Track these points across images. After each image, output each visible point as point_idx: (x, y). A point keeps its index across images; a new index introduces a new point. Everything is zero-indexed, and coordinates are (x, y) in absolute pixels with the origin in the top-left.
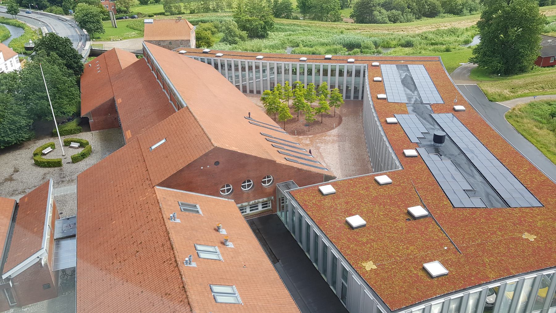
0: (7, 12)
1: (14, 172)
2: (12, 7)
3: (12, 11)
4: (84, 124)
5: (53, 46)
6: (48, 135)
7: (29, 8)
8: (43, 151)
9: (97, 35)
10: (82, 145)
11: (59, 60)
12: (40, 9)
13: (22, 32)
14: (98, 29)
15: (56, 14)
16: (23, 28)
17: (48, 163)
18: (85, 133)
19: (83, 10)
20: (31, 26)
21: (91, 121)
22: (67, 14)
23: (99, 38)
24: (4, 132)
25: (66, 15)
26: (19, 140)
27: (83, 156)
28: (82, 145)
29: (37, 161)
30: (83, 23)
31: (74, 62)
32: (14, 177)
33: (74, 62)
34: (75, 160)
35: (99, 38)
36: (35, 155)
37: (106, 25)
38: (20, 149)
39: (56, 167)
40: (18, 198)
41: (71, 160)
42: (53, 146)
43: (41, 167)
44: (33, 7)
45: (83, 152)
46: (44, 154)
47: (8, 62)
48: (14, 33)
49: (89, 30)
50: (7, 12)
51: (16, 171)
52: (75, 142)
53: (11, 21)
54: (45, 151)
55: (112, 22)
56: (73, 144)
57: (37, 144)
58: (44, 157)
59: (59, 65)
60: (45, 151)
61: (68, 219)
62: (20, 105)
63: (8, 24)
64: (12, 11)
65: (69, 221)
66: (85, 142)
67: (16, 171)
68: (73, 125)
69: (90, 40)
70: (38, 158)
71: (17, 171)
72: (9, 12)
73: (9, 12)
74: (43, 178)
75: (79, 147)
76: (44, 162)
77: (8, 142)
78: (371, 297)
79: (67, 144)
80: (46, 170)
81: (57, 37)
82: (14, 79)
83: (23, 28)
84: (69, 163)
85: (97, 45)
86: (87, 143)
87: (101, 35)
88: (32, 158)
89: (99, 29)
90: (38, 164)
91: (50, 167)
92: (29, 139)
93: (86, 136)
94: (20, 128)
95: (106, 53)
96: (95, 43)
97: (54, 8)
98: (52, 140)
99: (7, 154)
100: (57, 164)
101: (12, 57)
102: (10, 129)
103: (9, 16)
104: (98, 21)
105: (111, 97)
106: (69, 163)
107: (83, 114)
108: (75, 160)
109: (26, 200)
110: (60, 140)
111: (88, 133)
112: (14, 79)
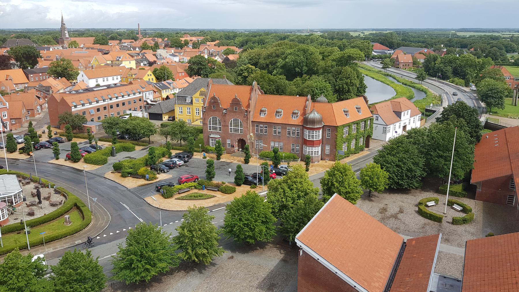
0: (416, 78)
1: (399, 212)
2: (422, 74)
3: (421, 78)
4: (470, 191)
5: (460, 114)
6: (433, 190)
7: (436, 77)
8: (428, 203)
9: (495, 109)
10: (465, 210)
11: (466, 127)
12: (444, 79)
13: (423, 95)
14: (498, 104)
15: (457, 85)
16: (426, 93)
17: (431, 215)
18: (468, 200)
19: (489, 85)
20: (433, 92)
21: (479, 190)
22: (467, 85)
23: (496, 113)
24: (401, 176)
25: (466, 87)
26: (409, 186)
27: (465, 221)
28: (465, 210)
29: (421, 210)
30: (484, 97)
31: (475, 131)
32: (400, 216)
33: (475, 131)
34: (455, 222)
35: (496, 113)
36: (420, 204)
37: (507, 101)
38: (407, 193)
39: (436, 221)
40: (406, 238)
41: (451, 221)
42: (437, 201)
43: (423, 216)
44: (439, 77)
45: (466, 217)
46: (427, 206)
47: (412, 119)
48: (418, 97)
49: (489, 104)
50: (416, 78)
51: (401, 211)
52: (458, 204)
53: (417, 85)
54: (430, 204)
55: (513, 100)
56: (455, 206)
57: (422, 195)
58: (426, 208)
59: (465, 131)
60: (430, 204)
61: (445, 277)
62: (421, 157)
63: (414, 87)
64: (421, 78)
65: (445, 280)
66: (468, 208)
67: (401, 211)
68: (459, 188)
69: (486, 113)
70: (422, 207)
71: (402, 212)
72: (418, 78)
73: (418, 78)
74: (423, 227)
75: (461, 211)
76: (427, 214)
77: (401, 185)
78: (76, 243)
79: (450, 204)
80: (427, 221)
81: (466, 106)
82: (422, 135)
83: (426, 93)
84: (448, 222)
85: (493, 119)
86: (470, 211)
87: (499, 111)
88: (417, 206)
89: (500, 105)
90: (420, 213)
91: (430, 219)
92: (417, 188)
93: (469, 203)
94: (414, 177)
95: (506, 129)
96: (491, 117)
97: (456, 79)
98: (436, 196)
99: (396, 195)
100: (438, 219)
101: (417, 115)
102: (406, 174)
103: (417, 81)
104: (501, 98)
105: (509, 173)
106: (448, 222)
107: (472, 182)
108: (455, 222)
109: (414, 242)
110: (447, 198)
111: (472, 200)
112: (422, 135)
